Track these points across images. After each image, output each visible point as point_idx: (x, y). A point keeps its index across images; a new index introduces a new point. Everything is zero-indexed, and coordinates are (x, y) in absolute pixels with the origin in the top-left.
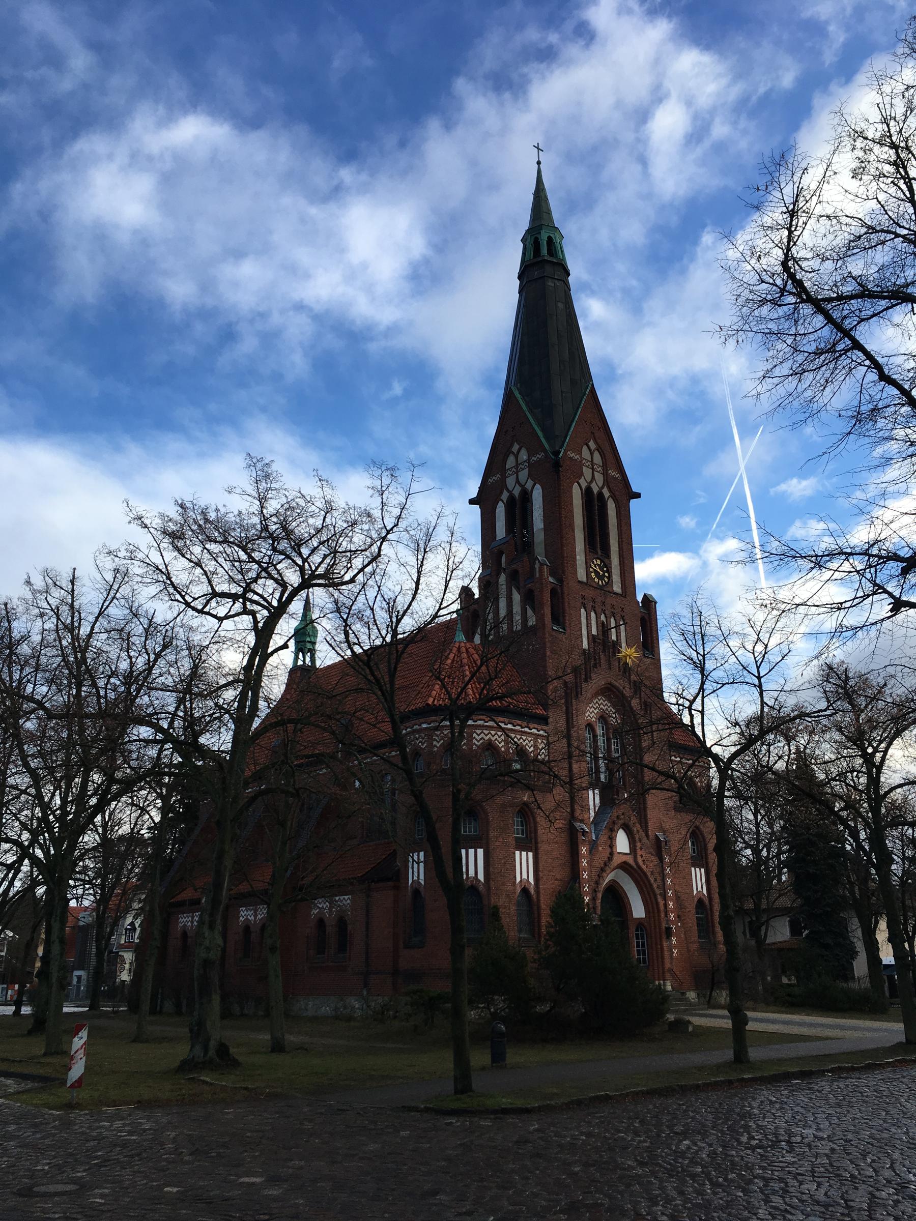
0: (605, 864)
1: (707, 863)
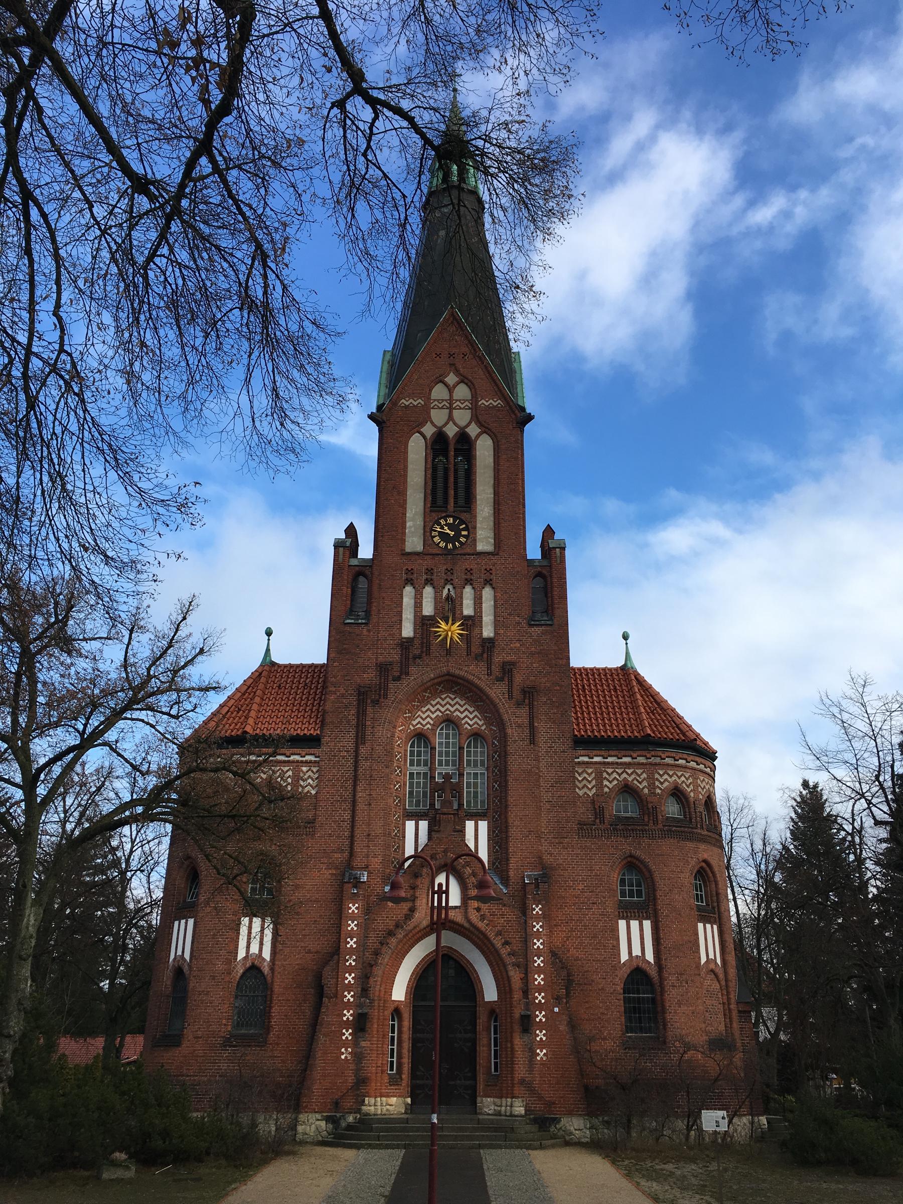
0: (397, 926)
1: (656, 911)
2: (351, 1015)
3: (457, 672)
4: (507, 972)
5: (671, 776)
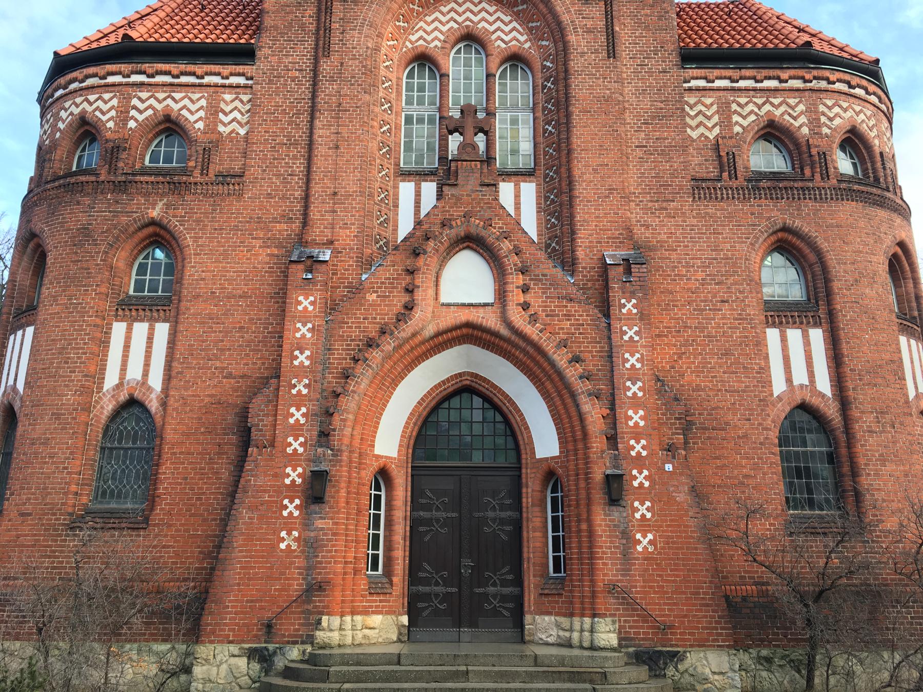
1: (831, 314)
2: (299, 476)
4: (577, 406)
5: (845, 110)
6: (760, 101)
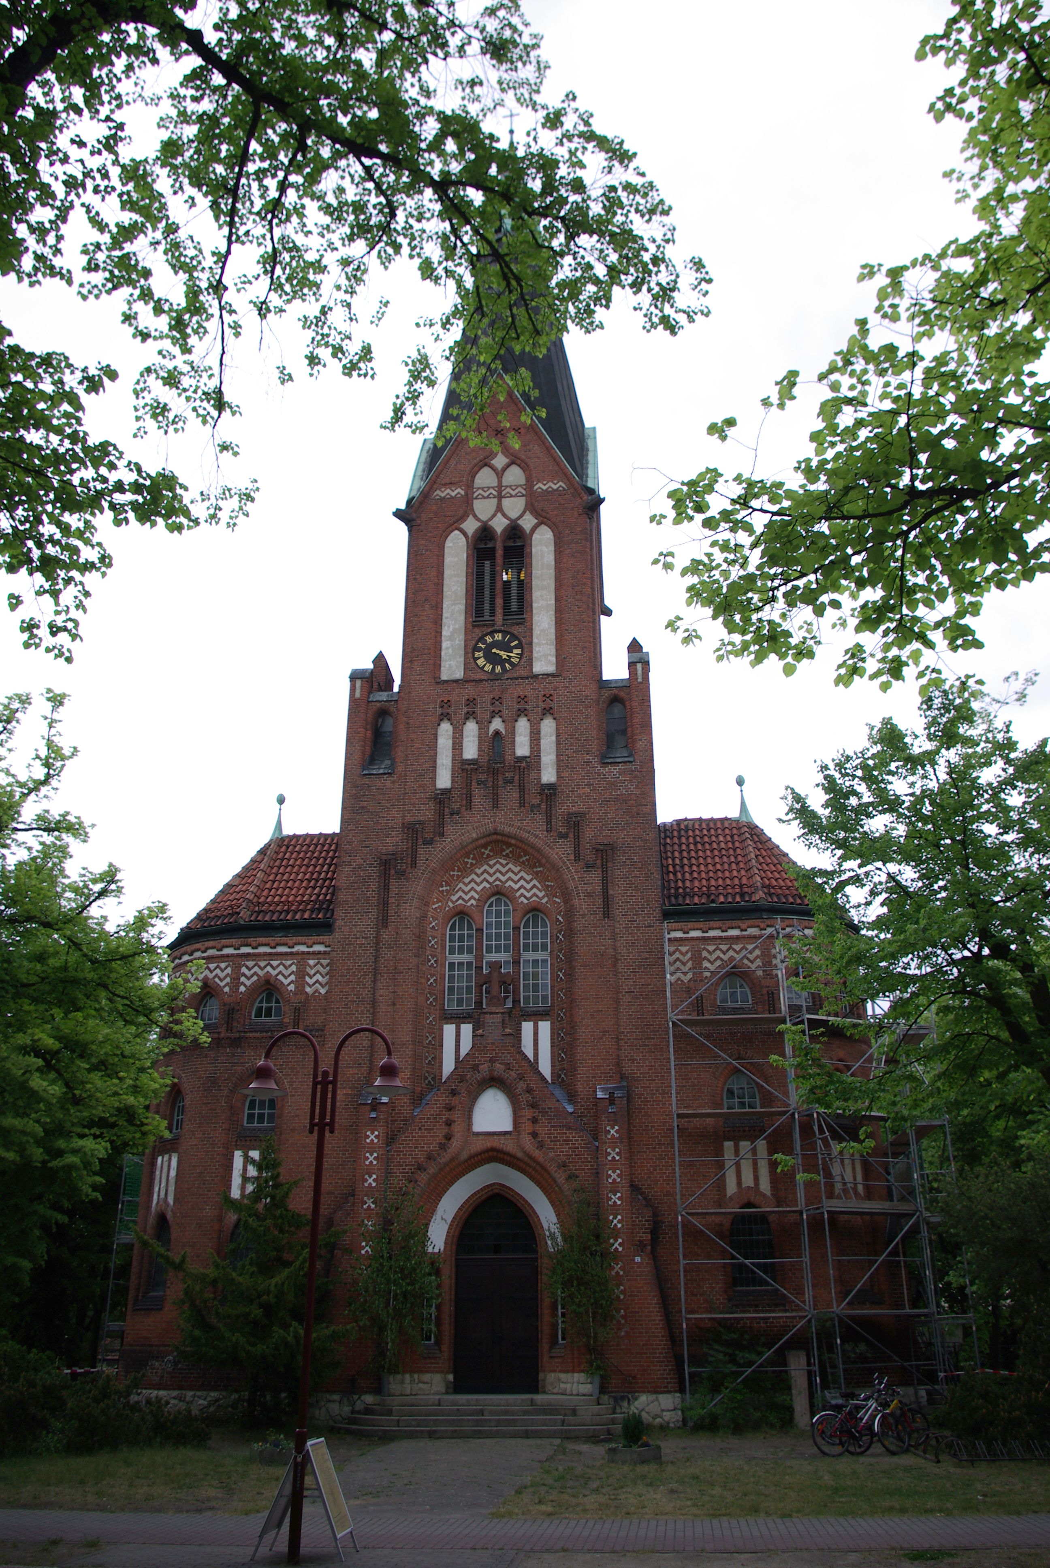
0: (429, 1158)
3: (507, 829)
6: (724, 947)
